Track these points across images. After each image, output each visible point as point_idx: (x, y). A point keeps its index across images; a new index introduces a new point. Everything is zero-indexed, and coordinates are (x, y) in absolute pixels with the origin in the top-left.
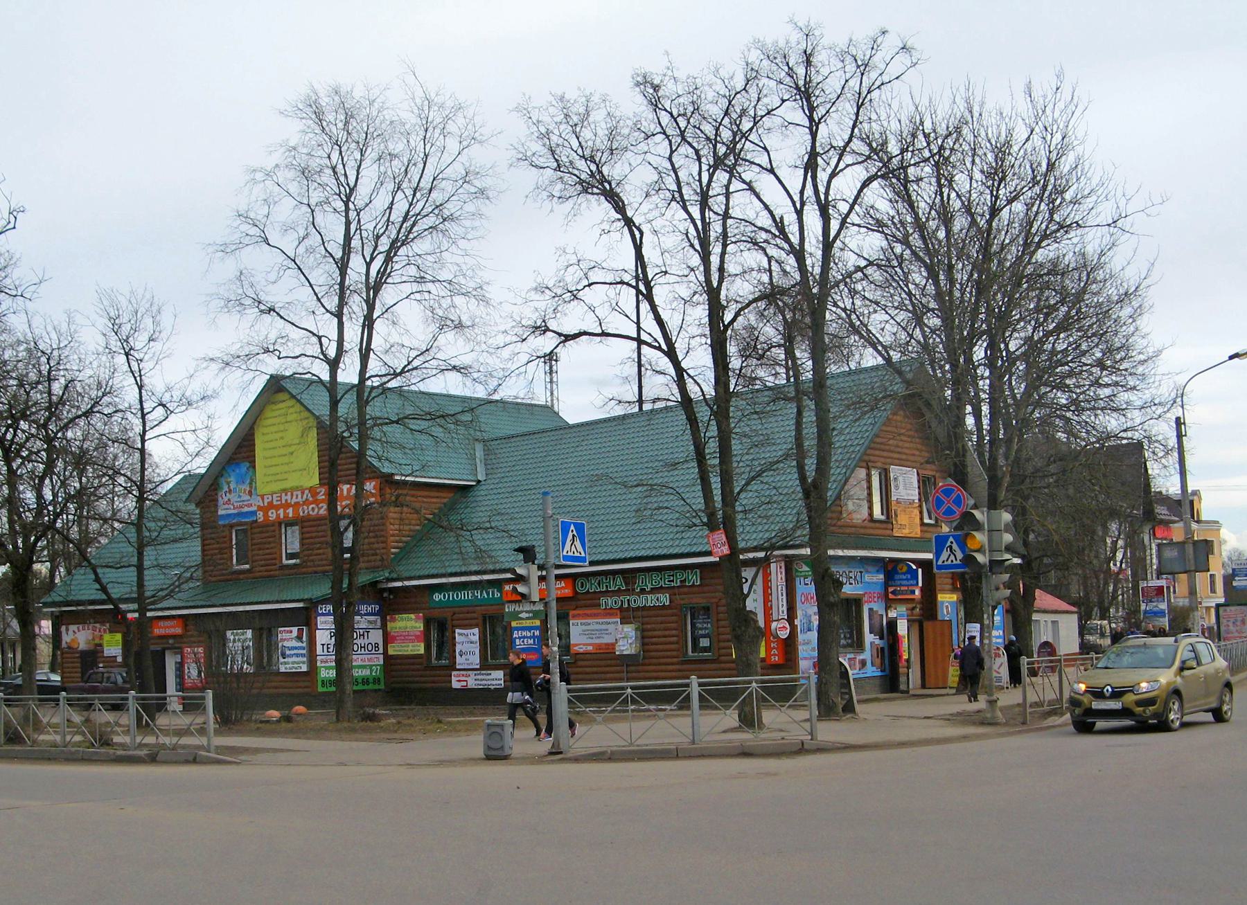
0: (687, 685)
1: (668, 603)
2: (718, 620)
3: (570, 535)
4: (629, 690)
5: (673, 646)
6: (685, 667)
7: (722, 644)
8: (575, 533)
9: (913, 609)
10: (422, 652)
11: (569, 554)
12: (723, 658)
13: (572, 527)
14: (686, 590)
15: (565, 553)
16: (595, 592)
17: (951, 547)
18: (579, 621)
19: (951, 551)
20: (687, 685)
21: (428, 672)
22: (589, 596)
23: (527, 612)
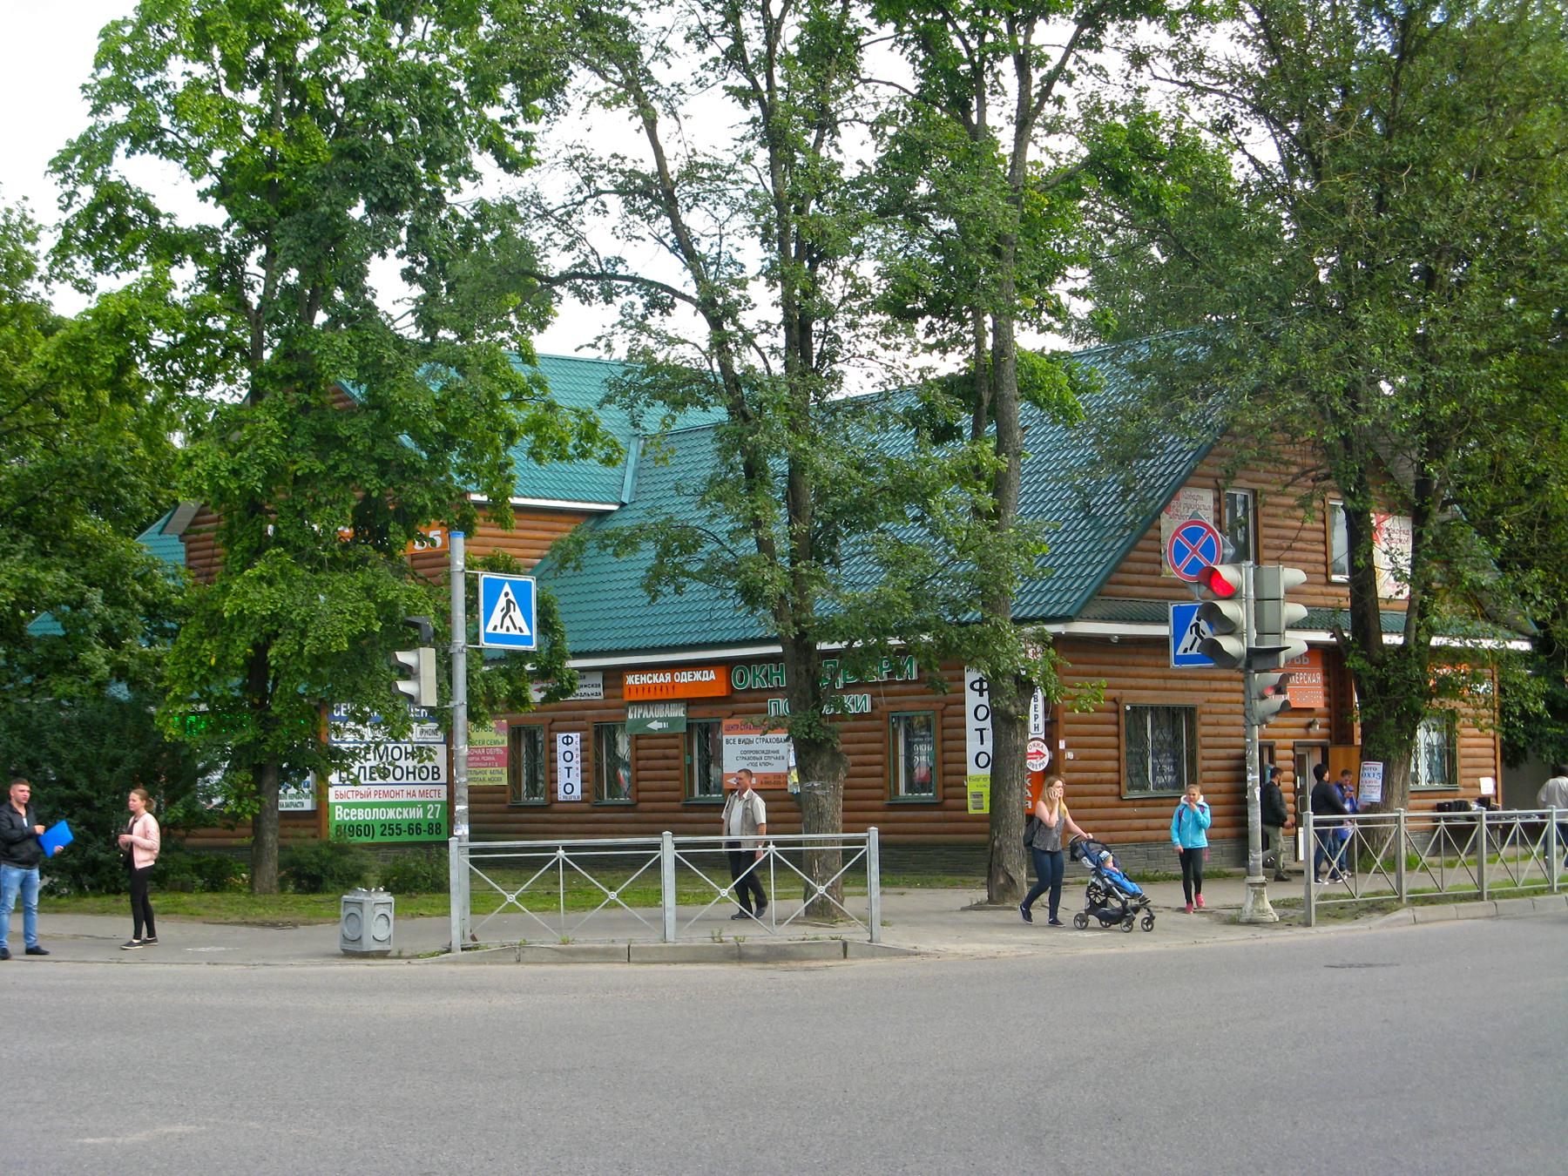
0: (657, 847)
1: (868, 710)
2: (943, 740)
3: (502, 602)
4: (561, 853)
5: (1106, 787)
6: (892, 815)
7: (949, 779)
8: (511, 597)
9: (1310, 725)
10: (505, 782)
11: (499, 631)
12: (950, 802)
13: (507, 588)
14: (897, 688)
15: (490, 630)
16: (760, 690)
17: (1197, 625)
18: (737, 737)
19: (1197, 632)
20: (657, 847)
21: (512, 816)
22: (754, 695)
23: (659, 720)
